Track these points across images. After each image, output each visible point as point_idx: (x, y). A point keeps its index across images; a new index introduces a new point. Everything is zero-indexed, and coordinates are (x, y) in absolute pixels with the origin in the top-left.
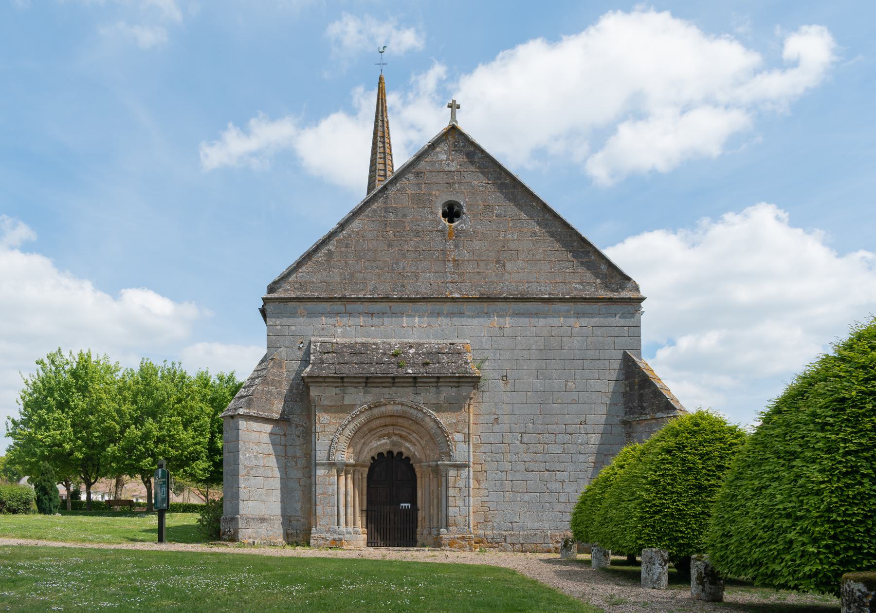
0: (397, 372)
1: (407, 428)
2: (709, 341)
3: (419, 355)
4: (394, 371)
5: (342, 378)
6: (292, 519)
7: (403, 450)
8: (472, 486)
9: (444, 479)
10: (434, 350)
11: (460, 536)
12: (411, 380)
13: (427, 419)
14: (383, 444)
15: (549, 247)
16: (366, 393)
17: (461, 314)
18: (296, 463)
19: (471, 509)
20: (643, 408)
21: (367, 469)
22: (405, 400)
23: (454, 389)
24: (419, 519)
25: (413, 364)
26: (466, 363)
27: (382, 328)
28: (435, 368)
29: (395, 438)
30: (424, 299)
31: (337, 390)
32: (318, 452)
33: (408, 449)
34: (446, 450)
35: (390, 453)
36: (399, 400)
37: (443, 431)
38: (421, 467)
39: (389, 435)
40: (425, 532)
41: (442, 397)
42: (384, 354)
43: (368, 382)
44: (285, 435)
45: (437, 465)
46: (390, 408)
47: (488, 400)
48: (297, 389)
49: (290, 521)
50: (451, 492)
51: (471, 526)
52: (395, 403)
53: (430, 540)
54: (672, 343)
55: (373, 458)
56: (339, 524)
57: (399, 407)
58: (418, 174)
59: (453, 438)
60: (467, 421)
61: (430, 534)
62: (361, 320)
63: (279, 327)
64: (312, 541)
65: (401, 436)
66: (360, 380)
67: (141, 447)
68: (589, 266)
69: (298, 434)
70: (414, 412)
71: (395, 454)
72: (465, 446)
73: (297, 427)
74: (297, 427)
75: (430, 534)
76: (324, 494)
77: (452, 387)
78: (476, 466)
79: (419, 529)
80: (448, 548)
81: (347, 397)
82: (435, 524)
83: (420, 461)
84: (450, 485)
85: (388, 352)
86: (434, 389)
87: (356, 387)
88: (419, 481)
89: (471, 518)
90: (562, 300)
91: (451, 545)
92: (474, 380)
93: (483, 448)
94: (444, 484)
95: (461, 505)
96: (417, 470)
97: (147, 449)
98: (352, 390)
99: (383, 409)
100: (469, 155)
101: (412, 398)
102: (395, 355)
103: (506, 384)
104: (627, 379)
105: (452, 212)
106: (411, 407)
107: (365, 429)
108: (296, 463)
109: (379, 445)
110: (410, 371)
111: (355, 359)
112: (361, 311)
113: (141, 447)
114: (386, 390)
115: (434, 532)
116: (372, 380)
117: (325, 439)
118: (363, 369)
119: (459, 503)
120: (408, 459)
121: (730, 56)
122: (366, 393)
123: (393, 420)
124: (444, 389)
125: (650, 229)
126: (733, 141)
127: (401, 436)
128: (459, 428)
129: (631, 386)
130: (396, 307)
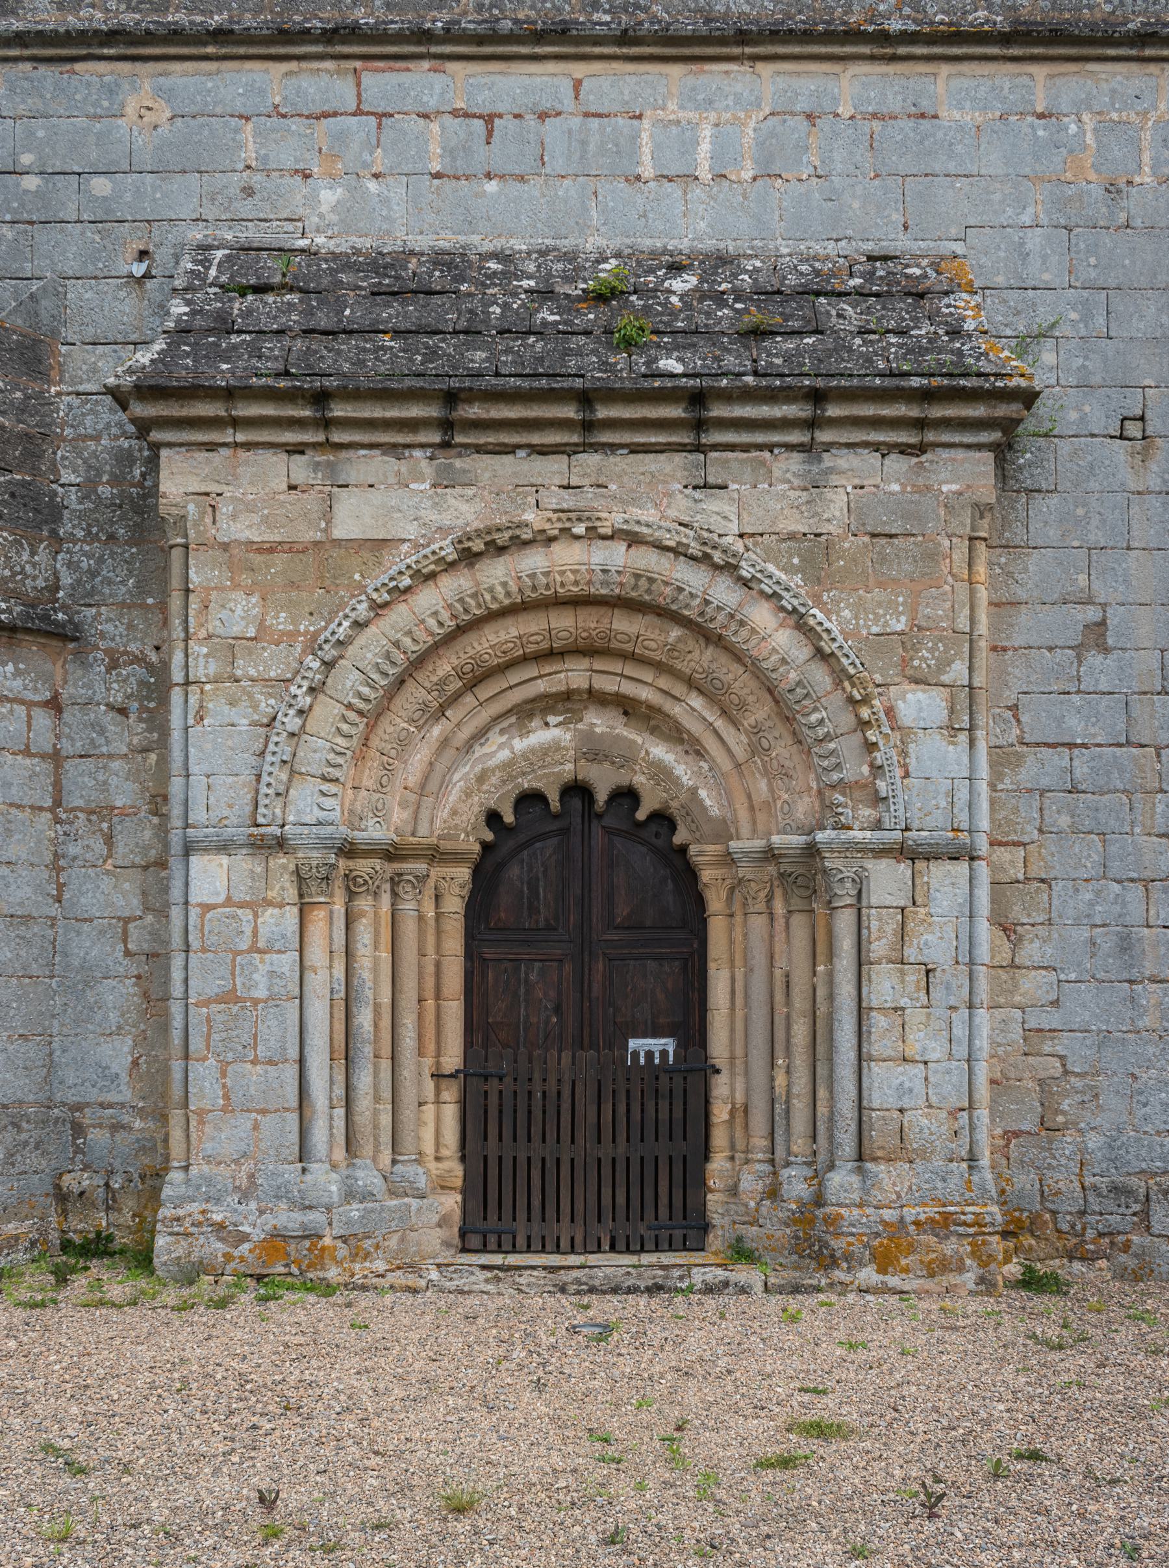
0: (605, 366)
1: (660, 667)
3: (719, 299)
4: (589, 363)
5: (321, 398)
6: (87, 1118)
7: (640, 780)
8: (983, 953)
9: (844, 922)
10: (792, 280)
11: (932, 1211)
12: (675, 412)
14: (545, 751)
18: (109, 840)
19: (982, 1072)
21: (463, 873)
22: (649, 514)
23: (897, 463)
24: (720, 1113)
25: (687, 337)
26: (955, 332)
27: (535, 187)
28: (799, 352)
29: (599, 722)
31: (300, 468)
32: (198, 782)
33: (661, 773)
34: (856, 769)
35: (577, 790)
36: (615, 519)
38: (728, 860)
39: (565, 702)
40: (751, 1183)
41: (836, 505)
42: (544, 294)
44: (54, 705)
45: (812, 851)
46: (568, 562)
47: (1053, 534)
48: (115, 481)
49: (78, 1129)
50: (884, 986)
51: (985, 1162)
52: (593, 534)
53: (773, 1228)
55: (493, 818)
56: (304, 1154)
57: (616, 555)
59: (890, 712)
60: (963, 624)
61: (773, 1193)
63: (31, 183)
64: (161, 1242)
65: (627, 707)
66: (415, 411)
69: (118, 698)
70: (693, 578)
71: (601, 797)
72: (955, 754)
73: (113, 665)
74: (113, 665)
75: (773, 1193)
76: (229, 997)
77: (883, 450)
78: (1003, 855)
79: (718, 1165)
80: (868, 1275)
82: (800, 1145)
83: (723, 831)
84: (878, 948)
85: (562, 289)
86: (793, 463)
87: (393, 449)
88: (717, 929)
89: (983, 1115)
91: (884, 1262)
92: (1002, 410)
93: (1039, 768)
94: (846, 944)
95: (936, 1051)
96: (706, 875)
98: (368, 466)
99: (534, 561)
101: (681, 506)
102: (601, 297)
103: (1145, 456)
106: (678, 551)
107: (445, 666)
108: (109, 840)
109: (542, 750)
110: (670, 364)
111: (390, 313)
112: (431, 102)
114: (552, 469)
115: (796, 1185)
116: (475, 411)
117: (232, 714)
118: (432, 354)
119: (919, 1041)
120: (663, 819)
122: (445, 481)
123: (587, 623)
124: (843, 460)
127: (627, 707)
128: (924, 660)
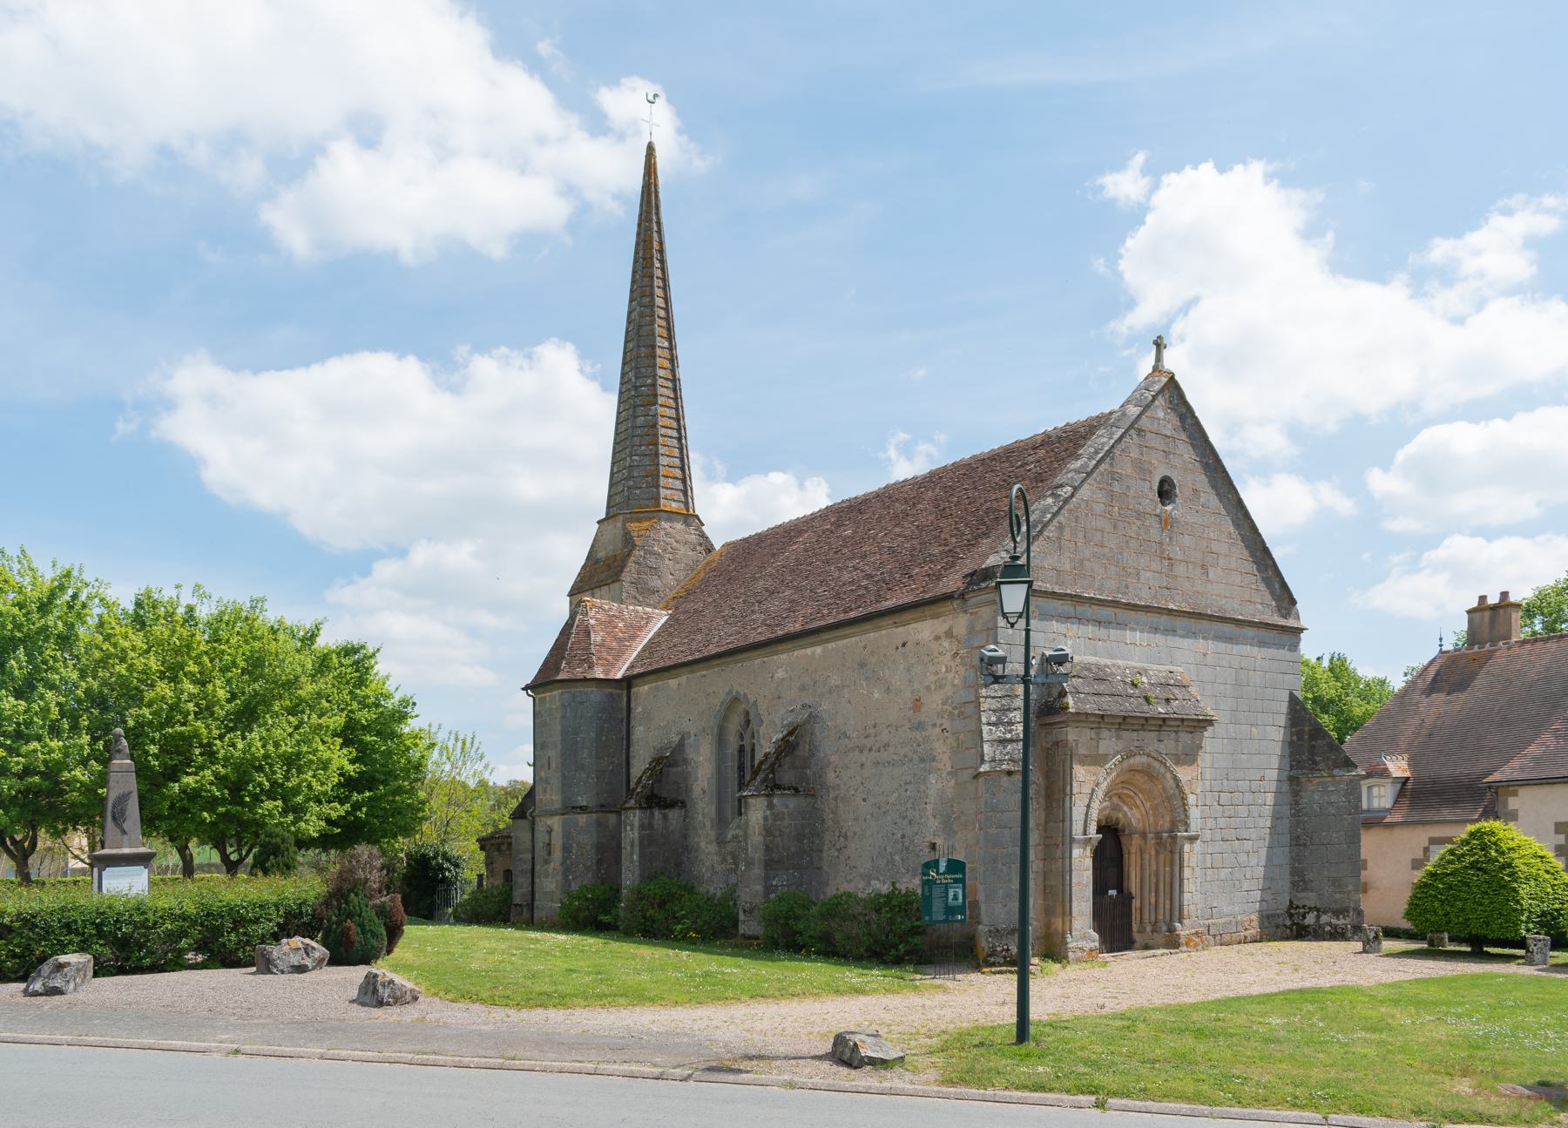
2: (460, 556)
13: (1168, 776)
15: (1238, 556)
16: (1118, 738)
17: (1173, 632)
20: (1315, 763)
30: (1147, 609)
37: (1181, 791)
43: (1124, 723)
54: (403, 553)
58: (1140, 432)
62: (1090, 630)
67: (260, 778)
68: (1267, 581)
81: (1102, 743)
90: (1251, 624)
97: (274, 784)
100: (1182, 418)
104: (1292, 726)
105: (1165, 491)
113: (260, 778)
121: (527, 99)
125: (374, 346)
126: (527, 241)
129: (1299, 734)
130: (1123, 615)
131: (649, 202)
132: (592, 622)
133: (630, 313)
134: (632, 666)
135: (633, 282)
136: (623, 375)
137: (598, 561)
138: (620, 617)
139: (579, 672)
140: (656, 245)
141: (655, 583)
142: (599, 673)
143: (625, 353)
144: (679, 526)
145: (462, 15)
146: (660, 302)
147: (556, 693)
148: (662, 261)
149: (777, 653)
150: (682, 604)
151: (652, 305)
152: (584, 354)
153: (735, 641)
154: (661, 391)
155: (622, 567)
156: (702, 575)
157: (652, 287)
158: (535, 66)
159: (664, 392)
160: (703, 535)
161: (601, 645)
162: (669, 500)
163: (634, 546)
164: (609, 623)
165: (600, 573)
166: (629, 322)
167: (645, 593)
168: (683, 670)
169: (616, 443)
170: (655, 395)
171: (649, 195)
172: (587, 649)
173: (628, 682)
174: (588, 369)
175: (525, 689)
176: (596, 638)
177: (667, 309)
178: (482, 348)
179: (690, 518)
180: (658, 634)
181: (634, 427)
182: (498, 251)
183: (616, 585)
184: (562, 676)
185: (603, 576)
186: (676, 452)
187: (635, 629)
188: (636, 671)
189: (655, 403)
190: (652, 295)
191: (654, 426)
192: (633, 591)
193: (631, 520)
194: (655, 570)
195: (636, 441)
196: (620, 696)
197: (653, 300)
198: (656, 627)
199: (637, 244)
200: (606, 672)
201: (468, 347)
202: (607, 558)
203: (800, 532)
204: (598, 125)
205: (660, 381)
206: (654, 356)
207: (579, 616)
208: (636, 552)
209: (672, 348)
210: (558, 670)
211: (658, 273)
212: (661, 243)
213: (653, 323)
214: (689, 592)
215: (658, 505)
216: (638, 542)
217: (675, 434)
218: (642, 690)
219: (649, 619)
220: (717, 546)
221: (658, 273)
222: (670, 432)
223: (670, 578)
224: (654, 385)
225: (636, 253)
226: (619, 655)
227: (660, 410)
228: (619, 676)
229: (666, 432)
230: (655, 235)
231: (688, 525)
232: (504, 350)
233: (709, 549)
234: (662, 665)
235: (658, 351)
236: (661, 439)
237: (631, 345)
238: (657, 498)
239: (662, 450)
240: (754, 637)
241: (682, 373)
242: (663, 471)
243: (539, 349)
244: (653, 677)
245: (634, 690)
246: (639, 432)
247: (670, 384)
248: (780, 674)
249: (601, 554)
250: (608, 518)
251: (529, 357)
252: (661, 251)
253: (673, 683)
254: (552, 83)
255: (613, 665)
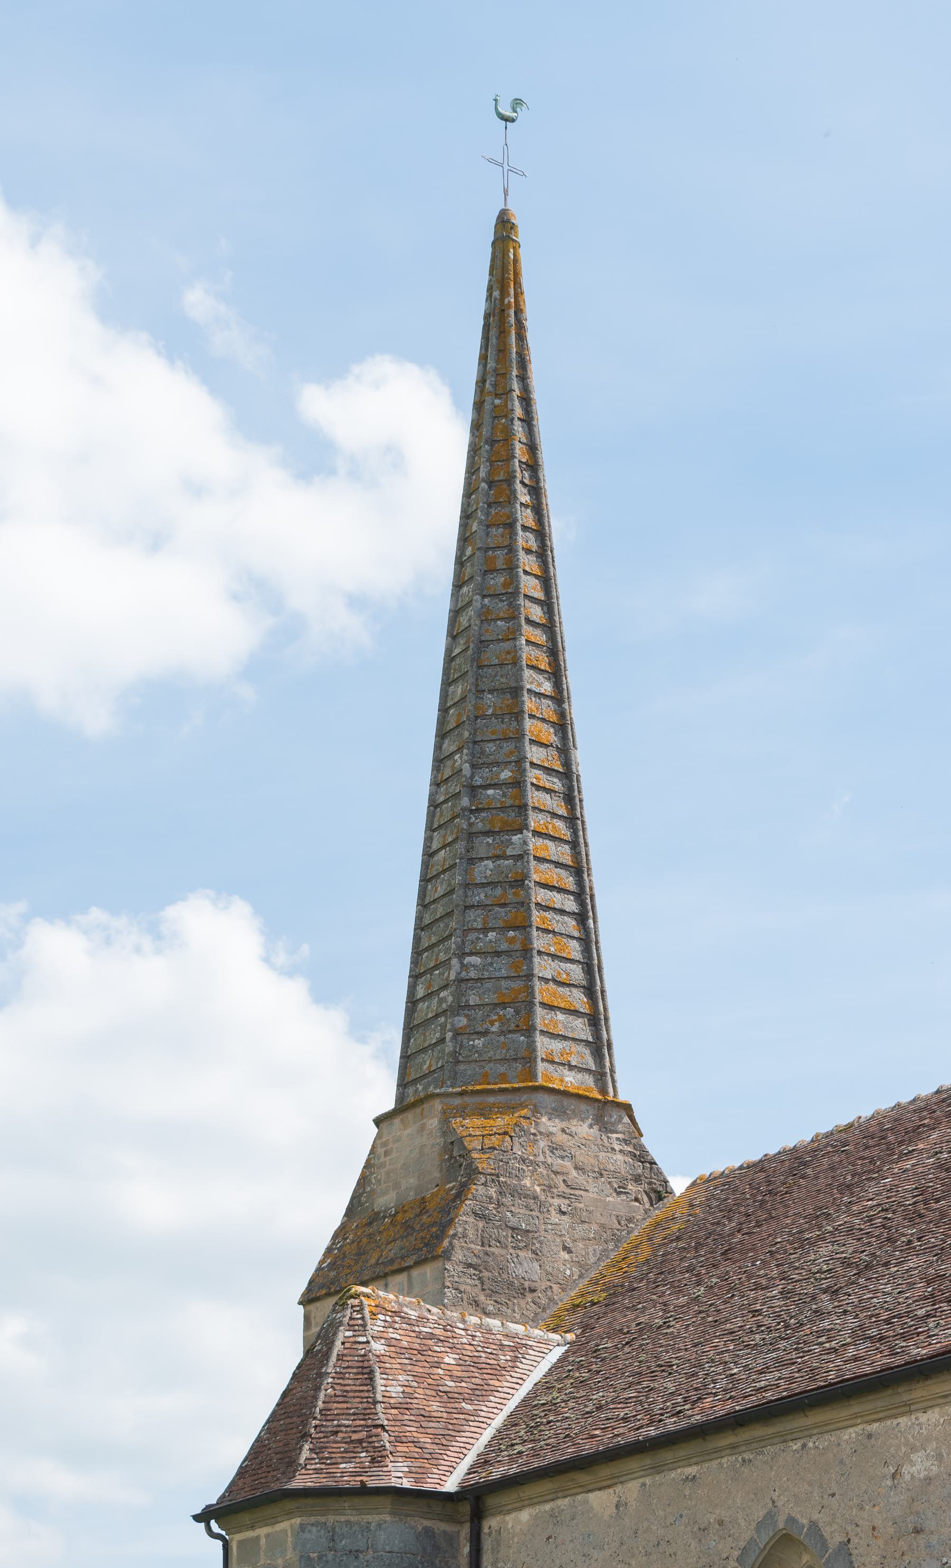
126: (160, 699)
131: (503, 351)
132: (378, 1347)
133: (455, 614)
134: (483, 1462)
135: (464, 539)
136: (439, 762)
137: (376, 1217)
138: (448, 1340)
139: (346, 1473)
140: (520, 451)
141: (526, 1268)
142: (398, 1474)
143: (444, 710)
144: (584, 1129)
145: (35, 241)
146: (530, 586)
147: (286, 1526)
148: (536, 491)
149: (908, 1409)
150: (599, 1318)
151: (512, 593)
152: (280, 927)
153: (775, 1384)
154: (534, 798)
155: (444, 1223)
156: (645, 1252)
157: (511, 549)
158: (180, 343)
159: (542, 801)
160: (642, 1156)
161: (403, 1407)
162: (558, 1060)
163: (473, 1172)
164: (420, 1353)
165: (388, 1237)
166: (453, 636)
167: (504, 1292)
168: (633, 1464)
169: (421, 927)
170: (522, 808)
171: (503, 333)
172: (367, 1413)
173: (475, 1501)
174: (281, 958)
175: (203, 1517)
176: (389, 1387)
177: (548, 604)
178: (59, 909)
179: (608, 1110)
180: (544, 1386)
181: (467, 886)
182: (97, 720)
183: (429, 1270)
184: (300, 1482)
185: (391, 1251)
186: (574, 949)
187: (480, 1375)
188: (497, 1472)
189: (522, 827)
190: (511, 568)
191: (520, 882)
192: (469, 1285)
193: (463, 1112)
194: (523, 1237)
195: (475, 918)
196: (452, 1540)
197: (513, 580)
198: (538, 1369)
199: (474, 451)
200: (419, 1474)
201: (21, 907)
202: (401, 1209)
203: (916, 1132)
204: (312, 458)
205: (533, 775)
206: (518, 715)
207: (344, 1334)
208: (478, 1190)
209: (559, 697)
210: (291, 1465)
211: (526, 517)
212: (532, 448)
213: (513, 635)
214: (614, 1292)
215: (532, 1075)
216: (483, 1163)
217: (570, 905)
218: (514, 1523)
219: (518, 1348)
220: (679, 1185)
221: (526, 517)
222: (558, 900)
223: (566, 1256)
224: (518, 783)
225: (472, 470)
226: (448, 1434)
227: (535, 845)
228: (451, 1485)
229: (547, 897)
230: (518, 427)
231: (606, 1129)
232: (97, 915)
233: (659, 1192)
234: (570, 1451)
235: (529, 704)
236: (536, 916)
237: (458, 690)
238: (528, 1059)
239: (539, 942)
240: (833, 1371)
241: (584, 759)
242: (541, 992)
243: (171, 912)
244: (545, 1486)
245: (491, 1523)
246: (480, 896)
247: (557, 784)
248: (919, 1466)
249: (386, 1200)
250: (403, 1107)
251: (155, 931)
252: (533, 467)
253: (600, 1501)
254: (213, 373)
255: (433, 1459)
